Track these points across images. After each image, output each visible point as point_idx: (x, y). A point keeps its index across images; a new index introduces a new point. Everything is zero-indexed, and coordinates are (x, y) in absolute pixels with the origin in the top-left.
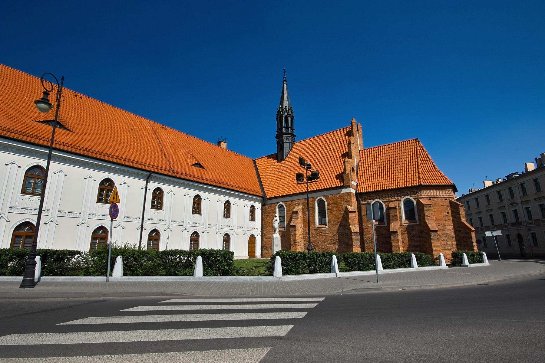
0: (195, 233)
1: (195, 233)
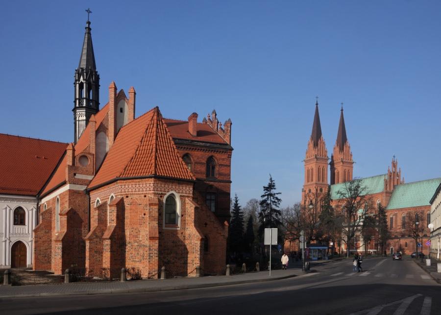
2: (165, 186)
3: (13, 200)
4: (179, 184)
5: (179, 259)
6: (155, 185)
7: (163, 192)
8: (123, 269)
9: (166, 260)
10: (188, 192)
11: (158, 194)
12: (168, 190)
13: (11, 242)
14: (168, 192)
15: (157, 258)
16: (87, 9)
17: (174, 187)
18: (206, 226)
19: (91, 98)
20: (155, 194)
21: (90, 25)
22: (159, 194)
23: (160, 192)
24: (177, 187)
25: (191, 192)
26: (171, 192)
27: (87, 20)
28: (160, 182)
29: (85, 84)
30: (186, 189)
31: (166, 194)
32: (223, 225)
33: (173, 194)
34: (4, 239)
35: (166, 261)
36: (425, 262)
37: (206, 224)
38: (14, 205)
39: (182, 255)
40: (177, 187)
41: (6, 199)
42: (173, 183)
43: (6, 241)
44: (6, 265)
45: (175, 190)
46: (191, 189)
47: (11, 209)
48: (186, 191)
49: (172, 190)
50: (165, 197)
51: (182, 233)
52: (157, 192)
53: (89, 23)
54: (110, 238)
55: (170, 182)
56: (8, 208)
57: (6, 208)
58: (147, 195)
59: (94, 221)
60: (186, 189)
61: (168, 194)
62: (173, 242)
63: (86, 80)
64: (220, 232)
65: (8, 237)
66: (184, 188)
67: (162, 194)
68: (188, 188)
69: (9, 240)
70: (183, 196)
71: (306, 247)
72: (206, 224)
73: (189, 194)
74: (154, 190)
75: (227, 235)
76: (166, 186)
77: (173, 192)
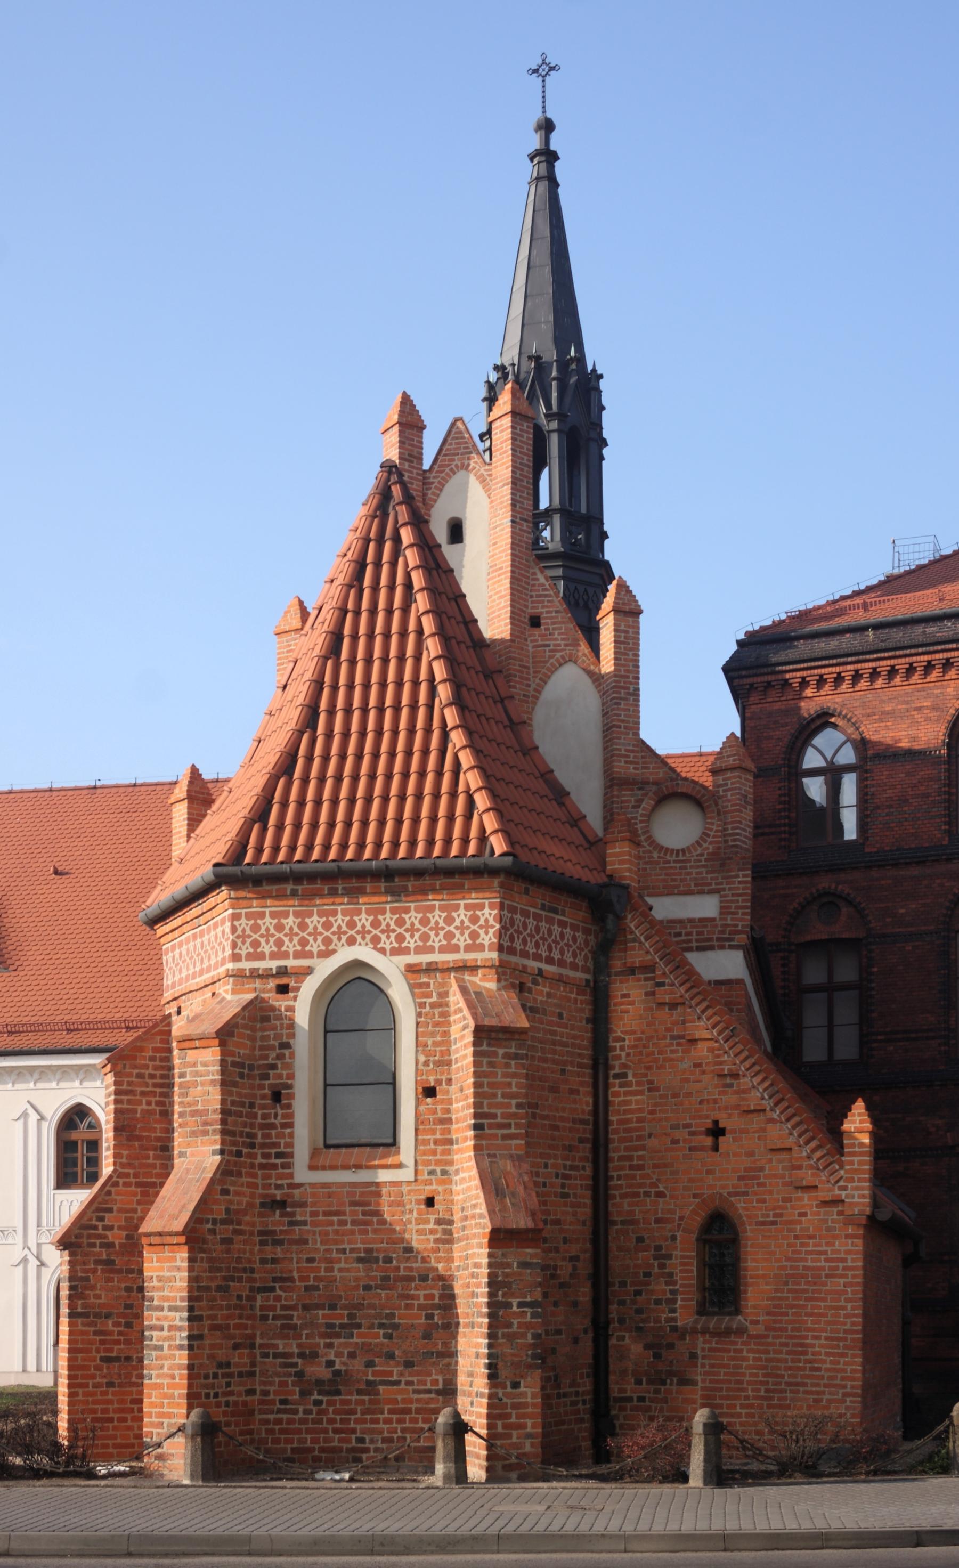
2: (303, 926)
3: (42, 1074)
4: (396, 893)
5: (409, 1364)
6: (243, 923)
7: (291, 963)
8: (443, 1418)
9: (319, 1371)
10: (462, 940)
11: (255, 974)
12: (327, 941)
13: (43, 1264)
14: (326, 954)
15: (182, 1358)
16: (535, 63)
17: (364, 920)
18: (716, 1148)
19: (544, 504)
20: (239, 975)
21: (554, 136)
22: (265, 975)
23: (274, 964)
24: (388, 919)
25: (488, 938)
26: (344, 955)
27: (537, 115)
28: (271, 906)
29: (554, 438)
30: (449, 920)
31: (309, 971)
32: (835, 1137)
33: (358, 964)
34: (18, 1253)
35: (324, 1373)
36: (19, 1454)
37: (717, 1132)
38: (56, 1098)
39: (427, 1336)
40: (388, 919)
41: (19, 1074)
42: (354, 893)
43: (25, 1260)
44: (24, 1371)
45: (375, 940)
46: (489, 914)
47: (42, 1118)
48: (449, 936)
49: (351, 942)
50: (308, 988)
51: (430, 1202)
52: (247, 965)
53: (547, 127)
54: (193, 1236)
55: (333, 893)
56: (31, 1111)
57: (25, 1115)
59: (108, 1149)
60: (449, 920)
61: (325, 968)
62: (368, 1258)
63: (560, 416)
64: (807, 1177)
65: (32, 1243)
66: (437, 916)
67: (283, 972)
68: (462, 915)
69: (38, 1258)
70: (431, 969)
71: (707, 1284)
72: (717, 1132)
73: (474, 947)
74: (236, 958)
75: (858, 1194)
76: (314, 921)
77: (363, 952)
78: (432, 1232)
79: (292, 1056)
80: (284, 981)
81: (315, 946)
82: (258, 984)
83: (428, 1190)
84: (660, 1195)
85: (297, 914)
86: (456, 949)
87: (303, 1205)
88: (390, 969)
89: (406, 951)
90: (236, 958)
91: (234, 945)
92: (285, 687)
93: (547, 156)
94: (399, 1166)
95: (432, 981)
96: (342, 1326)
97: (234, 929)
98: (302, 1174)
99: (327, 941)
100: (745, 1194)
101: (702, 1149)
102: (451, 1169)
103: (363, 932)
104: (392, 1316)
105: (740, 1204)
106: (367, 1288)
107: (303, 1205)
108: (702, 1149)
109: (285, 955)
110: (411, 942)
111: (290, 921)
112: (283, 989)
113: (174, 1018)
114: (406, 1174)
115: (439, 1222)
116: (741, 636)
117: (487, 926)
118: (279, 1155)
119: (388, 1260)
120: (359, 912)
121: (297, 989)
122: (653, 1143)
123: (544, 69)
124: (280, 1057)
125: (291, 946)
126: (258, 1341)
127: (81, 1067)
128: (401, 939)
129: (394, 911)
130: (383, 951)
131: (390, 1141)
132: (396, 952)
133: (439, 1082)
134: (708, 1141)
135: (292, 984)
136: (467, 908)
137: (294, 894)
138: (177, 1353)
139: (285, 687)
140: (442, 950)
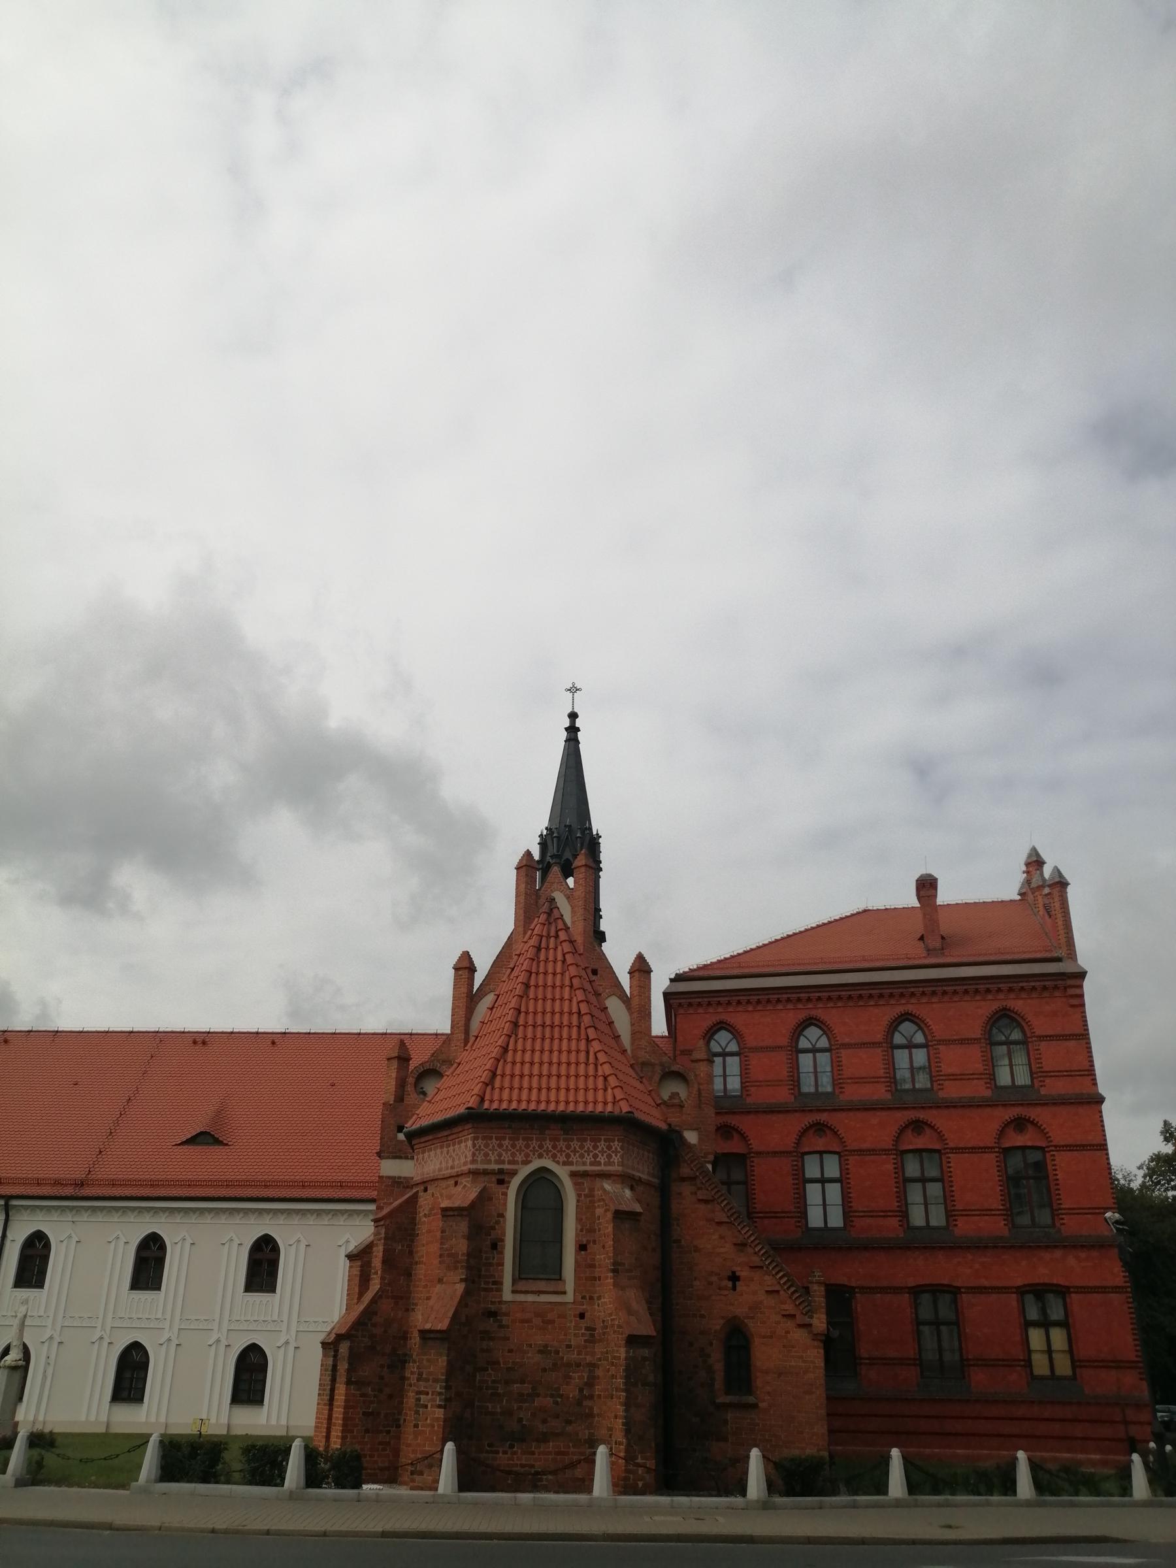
0: (136, 1347)
1: (136, 1347)
7: (506, 1166)
11: (485, 1173)
12: (527, 1155)
14: (526, 1162)
17: (548, 1144)
18: (734, 1288)
22: (492, 1172)
23: (496, 1167)
31: (514, 1173)
37: (734, 1278)
40: (562, 1144)
45: (554, 1157)
49: (540, 1156)
51: (582, 1316)
53: (573, 716)
58: (459, 1180)
60: (595, 1147)
61: (525, 1171)
67: (501, 1171)
70: (585, 1174)
78: (583, 1335)
79: (505, 1222)
80: (501, 1177)
81: (520, 1158)
82: (486, 1178)
83: (582, 1308)
84: (702, 1316)
85: (510, 1139)
86: (599, 1164)
87: (507, 1314)
88: (562, 1172)
89: (571, 1164)
90: (473, 1161)
91: (474, 1154)
92: (491, 1009)
93: (573, 730)
94: (565, 1293)
95: (586, 1183)
96: (528, 1395)
97: (474, 1145)
98: (507, 1295)
99: (527, 1155)
100: (752, 1318)
101: (726, 1288)
102: (595, 1296)
103: (548, 1151)
104: (559, 1389)
105: (751, 1324)
106: (544, 1370)
107: (507, 1314)
108: (726, 1288)
109: (503, 1162)
110: (573, 1158)
111: (506, 1142)
112: (501, 1182)
113: (421, 1194)
114: (569, 1297)
115: (587, 1329)
116: (673, 976)
117: (616, 1152)
118: (495, 1283)
119: (557, 1352)
120: (545, 1140)
121: (509, 1182)
122: (697, 1283)
123: (573, 690)
124: (498, 1222)
125: (506, 1157)
126: (476, 1403)
127: (227, 1209)
128: (568, 1156)
129: (565, 1140)
130: (558, 1163)
131: (557, 1277)
132: (564, 1164)
133: (588, 1241)
134: (730, 1284)
135: (506, 1179)
136: (605, 1141)
137: (509, 1127)
138: (437, 1410)
139: (491, 1009)
140: (592, 1164)
